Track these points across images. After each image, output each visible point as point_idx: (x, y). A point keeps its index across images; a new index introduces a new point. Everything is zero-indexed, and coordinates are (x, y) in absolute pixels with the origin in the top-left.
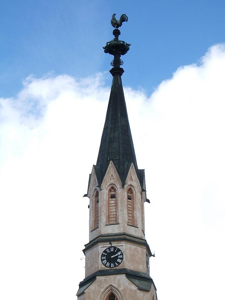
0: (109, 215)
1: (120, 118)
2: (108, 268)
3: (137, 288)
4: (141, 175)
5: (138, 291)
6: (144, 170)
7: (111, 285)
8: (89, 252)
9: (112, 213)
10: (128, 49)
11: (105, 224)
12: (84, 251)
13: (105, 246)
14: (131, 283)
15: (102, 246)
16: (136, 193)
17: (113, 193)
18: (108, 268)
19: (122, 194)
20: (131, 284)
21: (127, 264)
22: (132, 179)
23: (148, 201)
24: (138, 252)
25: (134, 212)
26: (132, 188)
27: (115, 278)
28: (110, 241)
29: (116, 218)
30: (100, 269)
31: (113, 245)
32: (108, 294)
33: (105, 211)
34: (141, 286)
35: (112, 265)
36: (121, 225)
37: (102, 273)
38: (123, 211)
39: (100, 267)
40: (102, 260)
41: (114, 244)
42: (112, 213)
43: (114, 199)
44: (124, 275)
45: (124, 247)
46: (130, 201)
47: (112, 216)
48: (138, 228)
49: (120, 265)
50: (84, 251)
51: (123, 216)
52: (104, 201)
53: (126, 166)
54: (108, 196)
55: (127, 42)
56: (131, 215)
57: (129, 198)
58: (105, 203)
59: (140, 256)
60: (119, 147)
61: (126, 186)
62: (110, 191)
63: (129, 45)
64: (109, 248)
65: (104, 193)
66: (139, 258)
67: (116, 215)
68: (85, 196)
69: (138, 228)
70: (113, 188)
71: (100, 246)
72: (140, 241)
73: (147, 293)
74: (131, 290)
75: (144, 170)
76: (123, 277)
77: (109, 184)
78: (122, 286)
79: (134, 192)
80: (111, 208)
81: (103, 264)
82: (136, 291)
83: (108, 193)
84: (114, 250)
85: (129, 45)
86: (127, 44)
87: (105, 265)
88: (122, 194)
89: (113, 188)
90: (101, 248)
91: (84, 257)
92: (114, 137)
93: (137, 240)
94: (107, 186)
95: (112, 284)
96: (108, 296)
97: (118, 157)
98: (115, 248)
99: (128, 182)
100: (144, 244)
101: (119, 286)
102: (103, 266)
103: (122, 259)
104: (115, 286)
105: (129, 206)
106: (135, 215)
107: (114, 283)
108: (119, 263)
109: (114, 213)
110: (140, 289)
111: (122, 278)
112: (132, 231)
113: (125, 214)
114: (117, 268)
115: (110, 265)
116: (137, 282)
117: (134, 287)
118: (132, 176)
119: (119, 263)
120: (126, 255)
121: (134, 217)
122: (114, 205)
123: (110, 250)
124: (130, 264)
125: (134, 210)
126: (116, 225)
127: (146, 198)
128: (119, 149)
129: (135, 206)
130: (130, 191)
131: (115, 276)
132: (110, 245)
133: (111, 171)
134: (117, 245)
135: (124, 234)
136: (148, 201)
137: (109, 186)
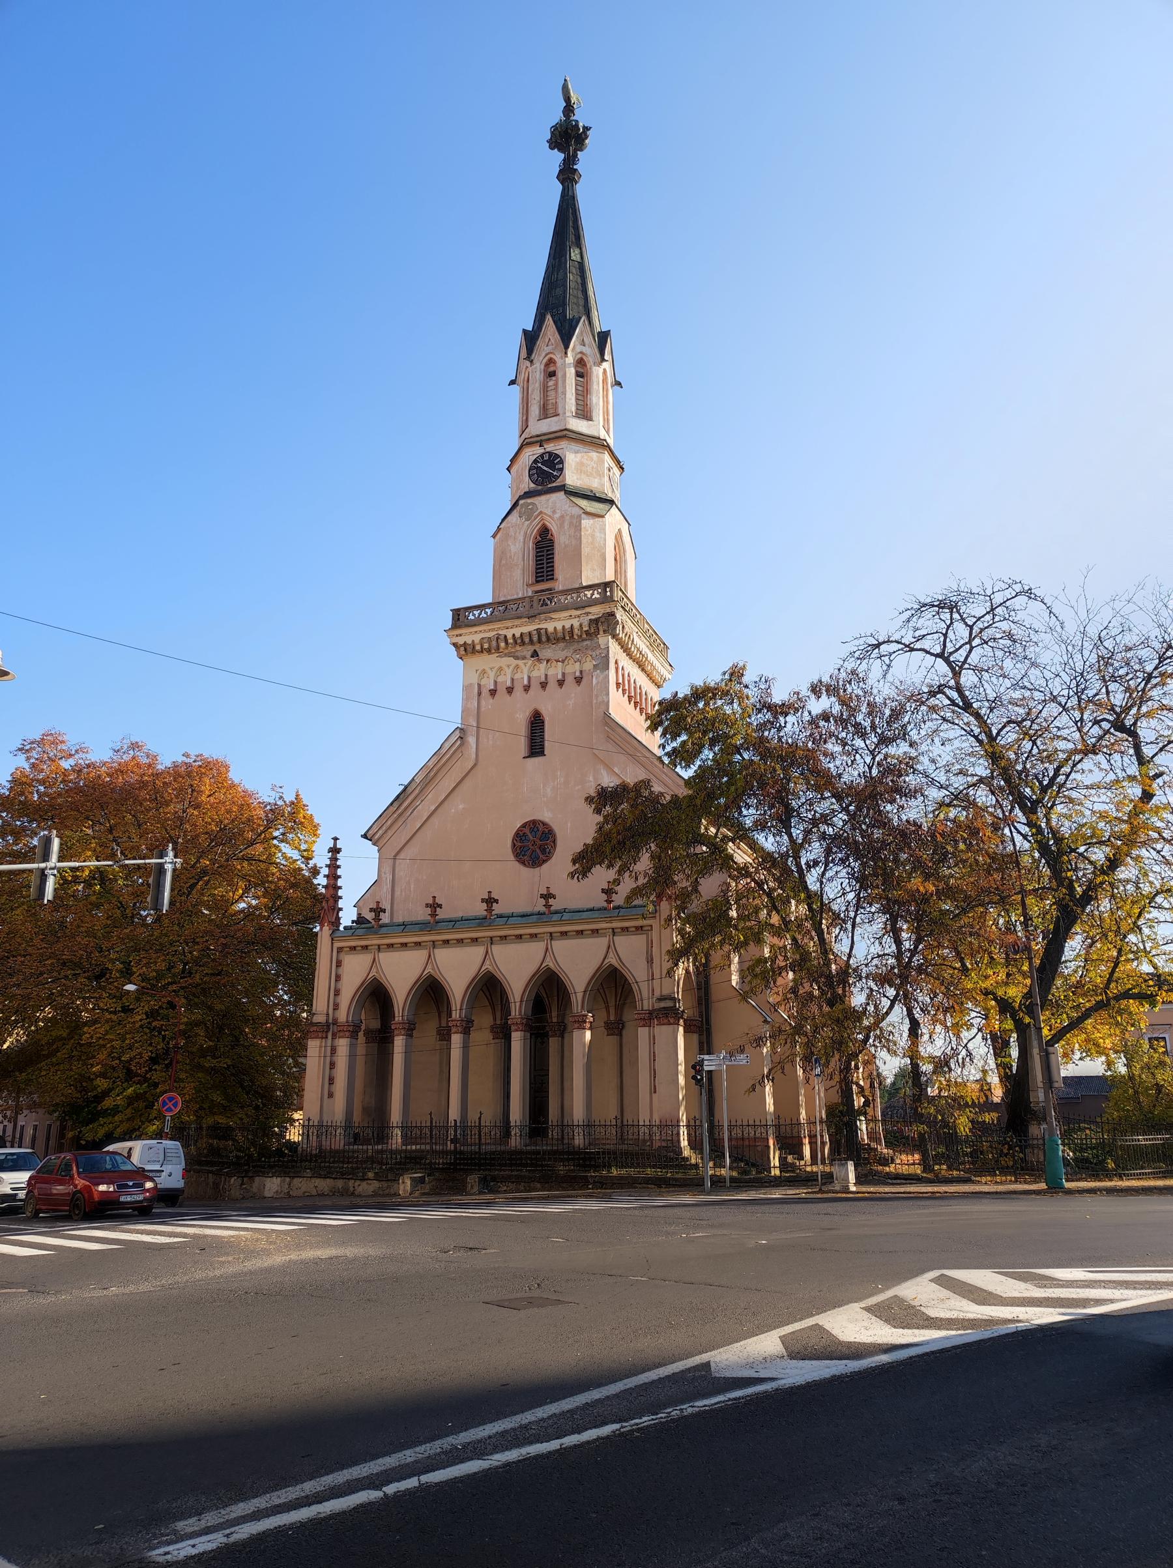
6: (609, 331)
8: (514, 470)
12: (508, 469)
13: (535, 452)
15: (531, 453)
26: (584, 358)
31: (548, 450)
41: (550, 447)
49: (558, 480)
55: (520, 332)
59: (595, 466)
66: (593, 467)
68: (513, 382)
77: (544, 354)
92: (557, 280)
94: (541, 358)
96: (538, 530)
98: (550, 454)
104: (549, 512)
105: (579, 388)
132: (543, 451)
133: (550, 329)
135: (566, 430)
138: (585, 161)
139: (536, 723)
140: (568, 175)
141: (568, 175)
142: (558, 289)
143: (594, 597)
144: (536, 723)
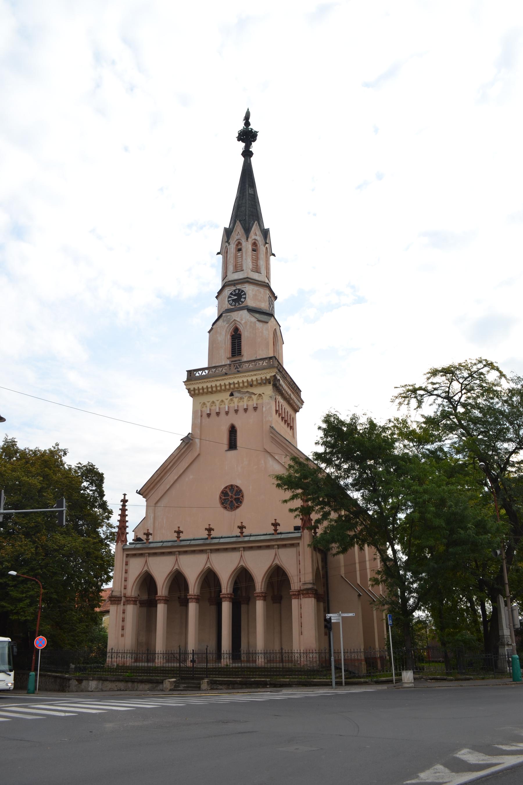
0: (235, 265)
1: (247, 188)
2: (233, 307)
3: (257, 320)
4: (266, 233)
5: (257, 322)
6: (269, 229)
7: (235, 320)
8: (220, 297)
9: (239, 263)
10: (257, 135)
11: (232, 272)
12: (217, 297)
13: (231, 289)
14: (252, 316)
15: (229, 290)
16: (260, 246)
17: (239, 247)
18: (233, 307)
19: (247, 246)
20: (252, 317)
21: (250, 302)
22: (255, 234)
23: (274, 255)
24: (261, 293)
25: (258, 261)
27: (238, 314)
28: (234, 285)
29: (241, 266)
30: (226, 308)
32: (232, 328)
33: (232, 262)
34: (260, 319)
35: (237, 304)
36: (245, 271)
37: (228, 311)
38: (247, 260)
39: (227, 306)
40: (229, 301)
41: (239, 287)
42: (239, 263)
43: (240, 252)
44: (246, 310)
45: (249, 289)
46: (255, 253)
47: (239, 266)
48: (261, 273)
49: (243, 304)
50: (217, 297)
51: (248, 263)
52: (231, 253)
53: (251, 224)
54: (236, 249)
56: (254, 264)
57: (254, 250)
58: (232, 255)
59: (262, 296)
60: (246, 210)
61: (249, 240)
62: (237, 245)
63: (257, 132)
64: (235, 291)
65: (232, 247)
66: (261, 297)
67: (242, 264)
68: (218, 253)
69: (261, 273)
70: (239, 244)
71: (227, 290)
72: (262, 283)
73: (266, 324)
74: (251, 322)
75: (269, 229)
76: (245, 312)
77: (235, 240)
78: (244, 319)
79: (258, 246)
80: (238, 259)
81: (229, 304)
82: (255, 322)
83: (236, 248)
84: (239, 291)
85: (257, 132)
86: (255, 131)
87: (231, 305)
88: (247, 246)
89: (239, 244)
90: (227, 292)
91: (217, 301)
92: (242, 203)
93: (259, 283)
94: (234, 242)
95: (236, 319)
96: (233, 329)
97: (244, 217)
98: (239, 290)
99: (252, 236)
100: (267, 286)
101: (242, 320)
102: (230, 306)
103: (245, 298)
104: (238, 320)
106: (259, 264)
107: (238, 318)
108: (243, 302)
109: (241, 263)
110: (259, 321)
111: (244, 313)
112: (255, 276)
113: (249, 262)
114: (241, 306)
115: (235, 304)
116: (257, 315)
117: (253, 319)
118: (257, 233)
119: (243, 302)
120: (249, 295)
121: (258, 265)
122: (240, 256)
123: (235, 292)
124: (252, 302)
125: (258, 260)
126: (241, 272)
127: (272, 252)
128: (246, 211)
129: (259, 256)
130: (255, 244)
131: (238, 312)
133: (239, 228)
134: (241, 287)
135: (247, 278)
136: (274, 255)
137: (236, 241)
138: (255, 147)
139: (233, 431)
140: (247, 154)
141: (247, 154)
142: (242, 208)
143: (202, 374)
144: (233, 431)
